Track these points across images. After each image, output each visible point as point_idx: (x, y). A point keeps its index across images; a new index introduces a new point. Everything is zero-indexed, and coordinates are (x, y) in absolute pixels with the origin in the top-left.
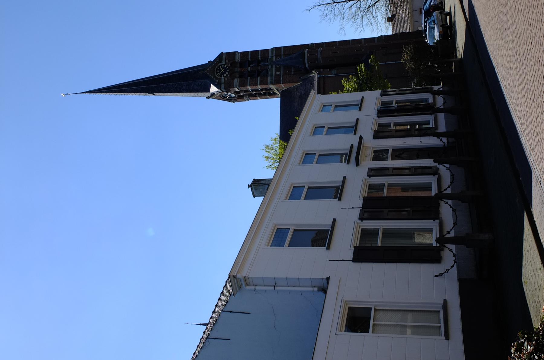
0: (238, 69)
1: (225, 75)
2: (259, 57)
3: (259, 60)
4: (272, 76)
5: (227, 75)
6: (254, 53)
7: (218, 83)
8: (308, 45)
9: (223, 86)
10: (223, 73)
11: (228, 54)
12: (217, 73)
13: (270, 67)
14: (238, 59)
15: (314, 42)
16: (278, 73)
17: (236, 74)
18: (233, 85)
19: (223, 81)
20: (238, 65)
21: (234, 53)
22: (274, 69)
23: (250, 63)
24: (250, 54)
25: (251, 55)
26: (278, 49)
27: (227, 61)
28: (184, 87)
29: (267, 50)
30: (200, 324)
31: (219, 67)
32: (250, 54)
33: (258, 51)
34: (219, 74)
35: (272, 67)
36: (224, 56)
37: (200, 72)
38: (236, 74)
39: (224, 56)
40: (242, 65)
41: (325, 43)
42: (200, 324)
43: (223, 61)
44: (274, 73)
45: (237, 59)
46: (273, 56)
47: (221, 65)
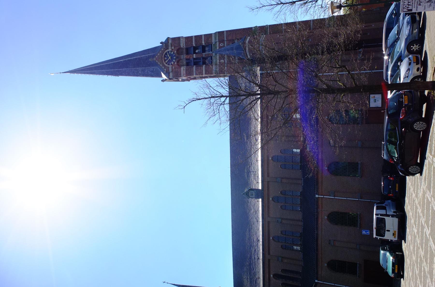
0: (184, 57)
1: (172, 63)
2: (203, 42)
3: (203, 46)
4: (216, 65)
5: (174, 62)
6: (198, 38)
7: (166, 72)
8: (251, 29)
9: (171, 74)
10: (170, 61)
11: (174, 39)
12: (165, 60)
13: (214, 54)
14: (183, 45)
15: (258, 26)
16: (222, 61)
17: (185, 57)
18: (180, 74)
19: (170, 69)
20: (185, 51)
21: (179, 38)
22: (218, 57)
23: (195, 48)
24: (213, 36)
25: (196, 41)
26: (220, 34)
27: (173, 48)
28: (140, 72)
29: (210, 35)
30: (174, 285)
31: (166, 54)
32: (312, 22)
33: (201, 36)
34: (167, 61)
35: (216, 54)
36: (170, 42)
37: (150, 60)
38: (185, 57)
39: (170, 42)
40: (188, 51)
41: (270, 26)
42: (174, 285)
43: (170, 48)
44: (218, 61)
45: (182, 45)
46: (216, 42)
47: (168, 52)
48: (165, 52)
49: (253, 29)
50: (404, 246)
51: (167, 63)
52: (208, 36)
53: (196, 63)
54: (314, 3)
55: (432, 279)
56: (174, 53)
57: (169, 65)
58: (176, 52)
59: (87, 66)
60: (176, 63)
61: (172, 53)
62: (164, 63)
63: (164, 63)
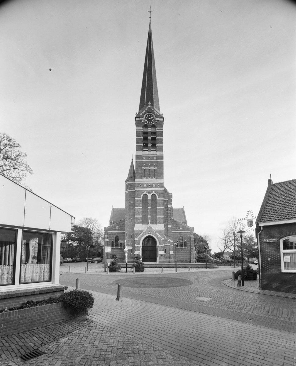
1: (146, 121)
5: (146, 122)
19: (141, 119)
27: (156, 121)
47: (154, 118)
48: (153, 114)
49: (171, 199)
50: (121, 204)
51: (146, 116)
52: (161, 149)
53: (146, 139)
54: (233, 245)
55: (132, 162)
56: (153, 122)
57: (145, 118)
58: (153, 124)
59: (22, 235)
60: (146, 123)
61: (153, 121)
62: (146, 114)
63: (146, 114)
